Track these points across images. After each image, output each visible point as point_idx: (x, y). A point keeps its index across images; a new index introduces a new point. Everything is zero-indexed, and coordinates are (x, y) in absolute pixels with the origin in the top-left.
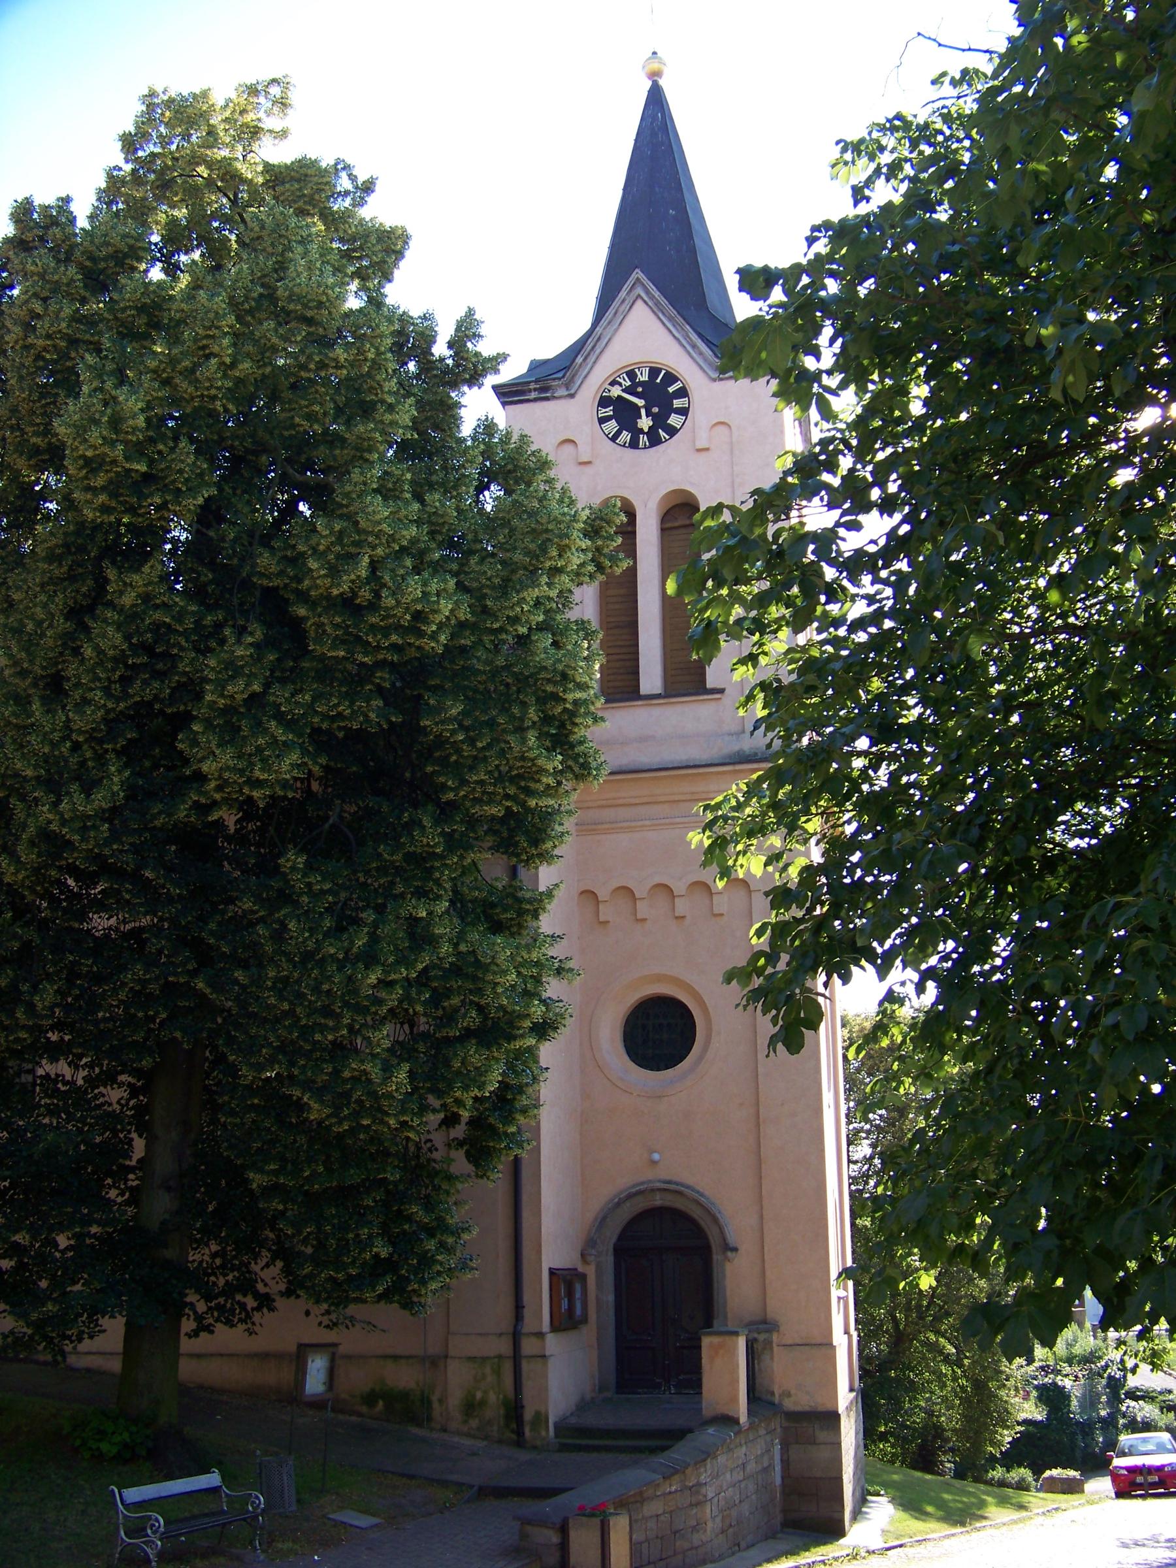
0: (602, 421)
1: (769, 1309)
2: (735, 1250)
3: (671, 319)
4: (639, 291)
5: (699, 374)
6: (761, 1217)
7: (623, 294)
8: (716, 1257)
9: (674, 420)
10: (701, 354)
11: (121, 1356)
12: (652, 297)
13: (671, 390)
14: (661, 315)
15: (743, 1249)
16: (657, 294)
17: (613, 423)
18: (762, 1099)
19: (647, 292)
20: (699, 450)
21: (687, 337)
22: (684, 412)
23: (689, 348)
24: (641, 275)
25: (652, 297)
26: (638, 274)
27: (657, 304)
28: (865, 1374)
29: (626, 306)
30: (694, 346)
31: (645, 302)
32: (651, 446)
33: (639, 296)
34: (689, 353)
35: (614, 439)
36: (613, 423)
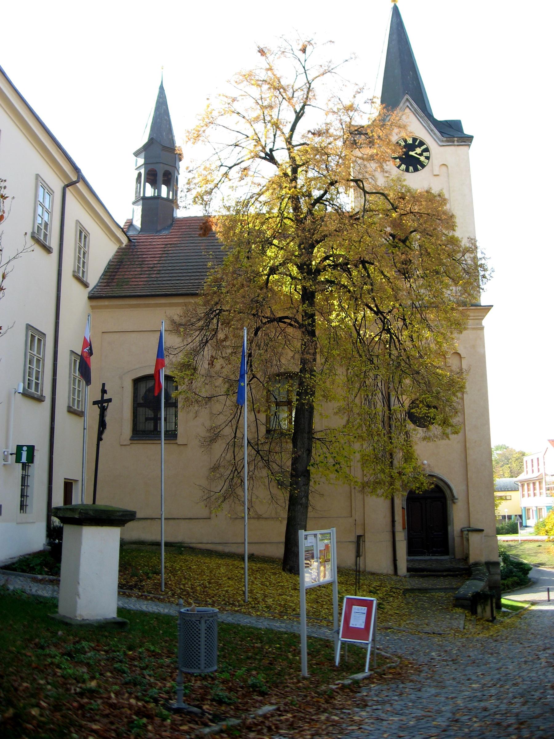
0: (399, 167)
1: (472, 520)
2: (457, 499)
4: (408, 104)
5: (434, 143)
6: (467, 486)
8: (449, 502)
9: (410, 141)
10: (435, 134)
11: (495, 487)
12: (413, 107)
16: (416, 106)
17: (403, 165)
18: (467, 440)
19: (411, 105)
20: (435, 175)
21: (429, 126)
23: (430, 131)
24: (409, 98)
25: (413, 107)
26: (407, 97)
27: (415, 110)
28: (352, 645)
30: (432, 130)
31: (410, 109)
32: (414, 172)
33: (408, 106)
34: (430, 133)
35: (399, 167)
36: (403, 165)
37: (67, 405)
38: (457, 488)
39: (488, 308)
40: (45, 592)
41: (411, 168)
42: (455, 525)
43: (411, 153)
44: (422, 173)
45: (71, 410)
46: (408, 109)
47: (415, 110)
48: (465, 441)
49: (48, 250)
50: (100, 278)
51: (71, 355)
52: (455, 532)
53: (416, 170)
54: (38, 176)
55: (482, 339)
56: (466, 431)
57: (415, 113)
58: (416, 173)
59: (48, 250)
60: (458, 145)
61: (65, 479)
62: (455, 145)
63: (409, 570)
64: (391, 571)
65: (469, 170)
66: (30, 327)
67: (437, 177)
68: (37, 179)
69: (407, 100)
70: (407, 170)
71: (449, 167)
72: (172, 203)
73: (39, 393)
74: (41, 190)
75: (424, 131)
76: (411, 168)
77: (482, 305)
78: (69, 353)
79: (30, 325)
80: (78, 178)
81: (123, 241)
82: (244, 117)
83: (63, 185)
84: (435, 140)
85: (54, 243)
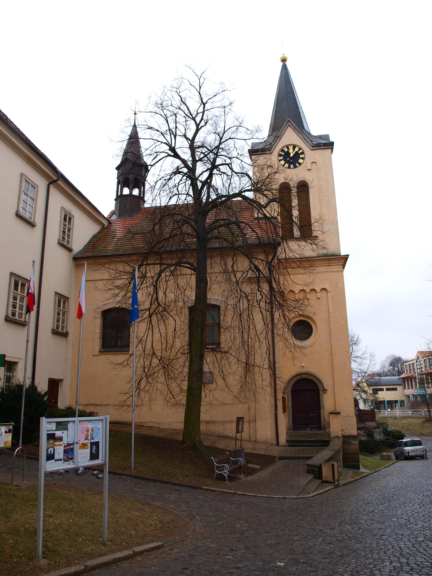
2: (327, 390)
3: (299, 132)
4: (289, 123)
7: (285, 124)
8: (321, 392)
10: (308, 142)
12: (293, 126)
13: (299, 152)
14: (296, 131)
15: (328, 390)
16: (294, 125)
17: (286, 164)
21: (304, 137)
22: (303, 159)
23: (304, 140)
24: (290, 119)
25: (293, 126)
27: (294, 127)
29: (286, 128)
30: (306, 140)
31: (291, 127)
33: (289, 125)
36: (286, 164)
37: (51, 328)
38: (327, 383)
39: (346, 258)
40: (38, 458)
41: (292, 166)
42: (325, 409)
43: (291, 155)
44: (299, 169)
45: (55, 332)
46: (289, 127)
47: (294, 127)
48: (332, 350)
49: (32, 225)
50: (85, 246)
51: (55, 295)
52: (326, 414)
53: (295, 167)
54: (22, 175)
55: (342, 278)
56: (332, 343)
57: (294, 129)
58: (295, 169)
59: (32, 225)
60: (324, 149)
61: (49, 378)
62: (321, 149)
63: (287, 441)
64: (275, 442)
65: (332, 165)
66: (13, 275)
67: (309, 171)
68: (21, 176)
69: (289, 120)
70: (289, 167)
71: (317, 162)
72: (141, 199)
73: (23, 320)
74: (24, 183)
75: (300, 140)
76: (292, 166)
77: (342, 255)
78: (54, 294)
79: (13, 273)
80: (58, 177)
81: (105, 223)
82: (158, 131)
83: (48, 183)
84: (308, 146)
85: (39, 221)
